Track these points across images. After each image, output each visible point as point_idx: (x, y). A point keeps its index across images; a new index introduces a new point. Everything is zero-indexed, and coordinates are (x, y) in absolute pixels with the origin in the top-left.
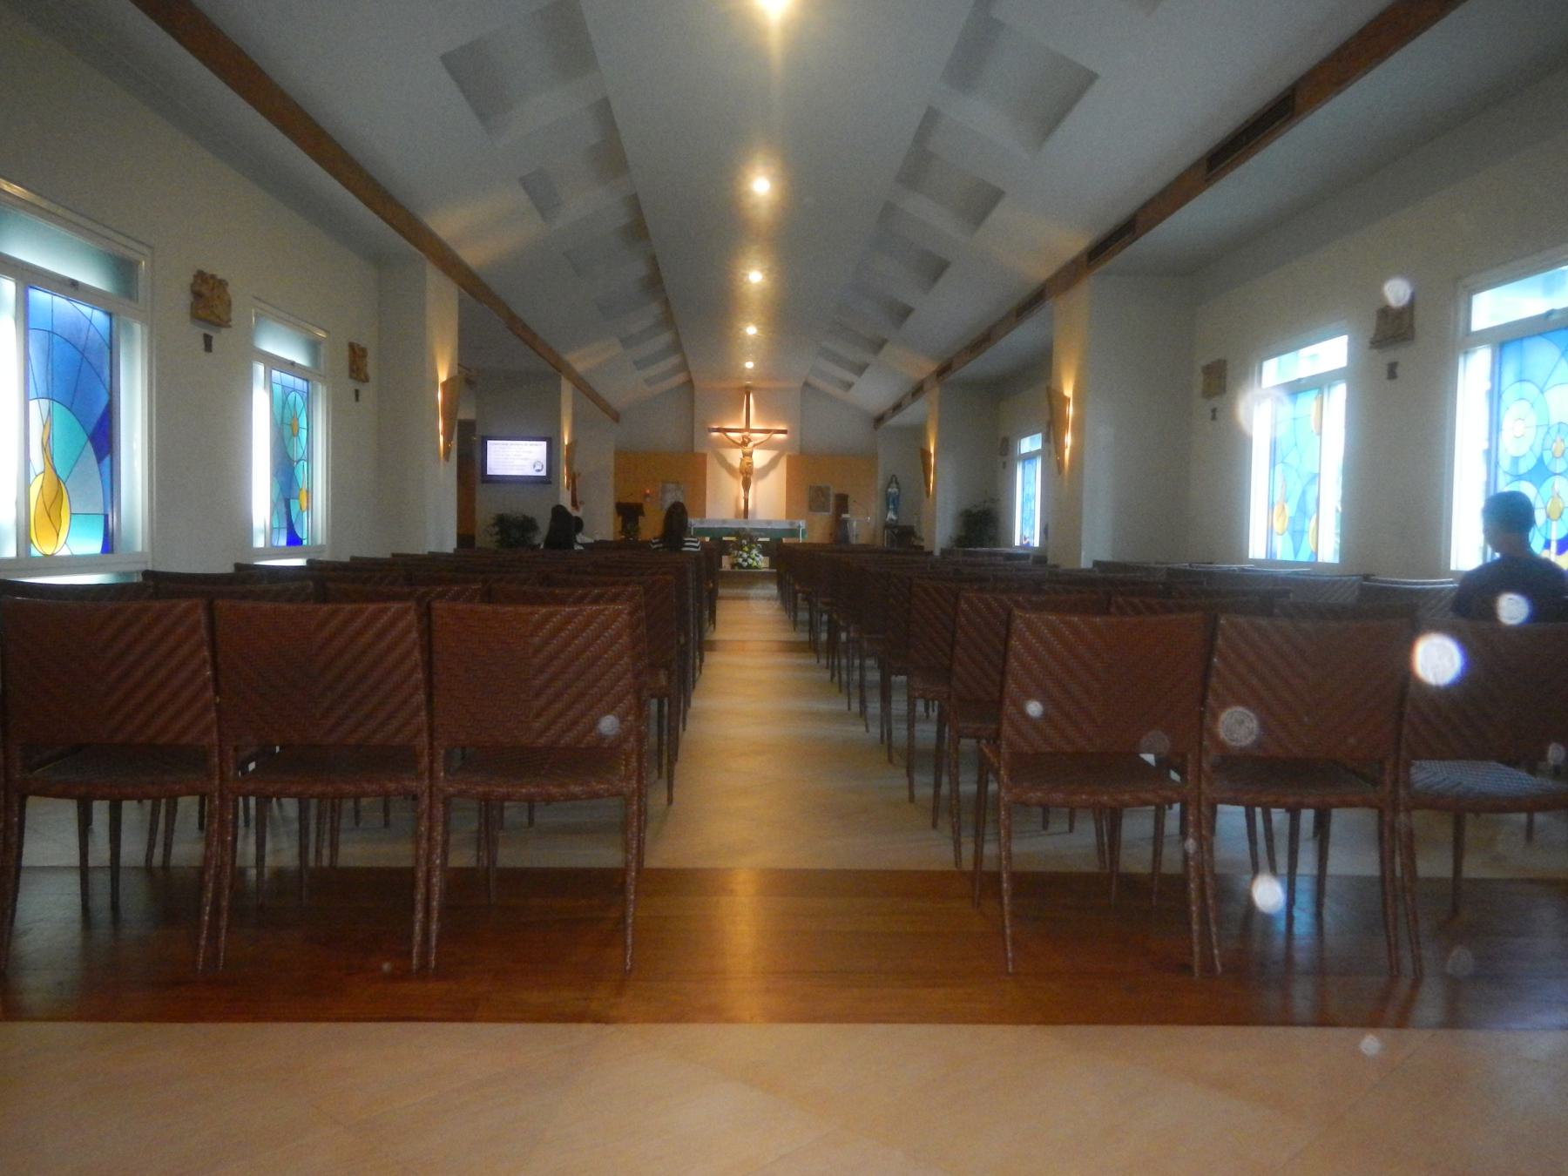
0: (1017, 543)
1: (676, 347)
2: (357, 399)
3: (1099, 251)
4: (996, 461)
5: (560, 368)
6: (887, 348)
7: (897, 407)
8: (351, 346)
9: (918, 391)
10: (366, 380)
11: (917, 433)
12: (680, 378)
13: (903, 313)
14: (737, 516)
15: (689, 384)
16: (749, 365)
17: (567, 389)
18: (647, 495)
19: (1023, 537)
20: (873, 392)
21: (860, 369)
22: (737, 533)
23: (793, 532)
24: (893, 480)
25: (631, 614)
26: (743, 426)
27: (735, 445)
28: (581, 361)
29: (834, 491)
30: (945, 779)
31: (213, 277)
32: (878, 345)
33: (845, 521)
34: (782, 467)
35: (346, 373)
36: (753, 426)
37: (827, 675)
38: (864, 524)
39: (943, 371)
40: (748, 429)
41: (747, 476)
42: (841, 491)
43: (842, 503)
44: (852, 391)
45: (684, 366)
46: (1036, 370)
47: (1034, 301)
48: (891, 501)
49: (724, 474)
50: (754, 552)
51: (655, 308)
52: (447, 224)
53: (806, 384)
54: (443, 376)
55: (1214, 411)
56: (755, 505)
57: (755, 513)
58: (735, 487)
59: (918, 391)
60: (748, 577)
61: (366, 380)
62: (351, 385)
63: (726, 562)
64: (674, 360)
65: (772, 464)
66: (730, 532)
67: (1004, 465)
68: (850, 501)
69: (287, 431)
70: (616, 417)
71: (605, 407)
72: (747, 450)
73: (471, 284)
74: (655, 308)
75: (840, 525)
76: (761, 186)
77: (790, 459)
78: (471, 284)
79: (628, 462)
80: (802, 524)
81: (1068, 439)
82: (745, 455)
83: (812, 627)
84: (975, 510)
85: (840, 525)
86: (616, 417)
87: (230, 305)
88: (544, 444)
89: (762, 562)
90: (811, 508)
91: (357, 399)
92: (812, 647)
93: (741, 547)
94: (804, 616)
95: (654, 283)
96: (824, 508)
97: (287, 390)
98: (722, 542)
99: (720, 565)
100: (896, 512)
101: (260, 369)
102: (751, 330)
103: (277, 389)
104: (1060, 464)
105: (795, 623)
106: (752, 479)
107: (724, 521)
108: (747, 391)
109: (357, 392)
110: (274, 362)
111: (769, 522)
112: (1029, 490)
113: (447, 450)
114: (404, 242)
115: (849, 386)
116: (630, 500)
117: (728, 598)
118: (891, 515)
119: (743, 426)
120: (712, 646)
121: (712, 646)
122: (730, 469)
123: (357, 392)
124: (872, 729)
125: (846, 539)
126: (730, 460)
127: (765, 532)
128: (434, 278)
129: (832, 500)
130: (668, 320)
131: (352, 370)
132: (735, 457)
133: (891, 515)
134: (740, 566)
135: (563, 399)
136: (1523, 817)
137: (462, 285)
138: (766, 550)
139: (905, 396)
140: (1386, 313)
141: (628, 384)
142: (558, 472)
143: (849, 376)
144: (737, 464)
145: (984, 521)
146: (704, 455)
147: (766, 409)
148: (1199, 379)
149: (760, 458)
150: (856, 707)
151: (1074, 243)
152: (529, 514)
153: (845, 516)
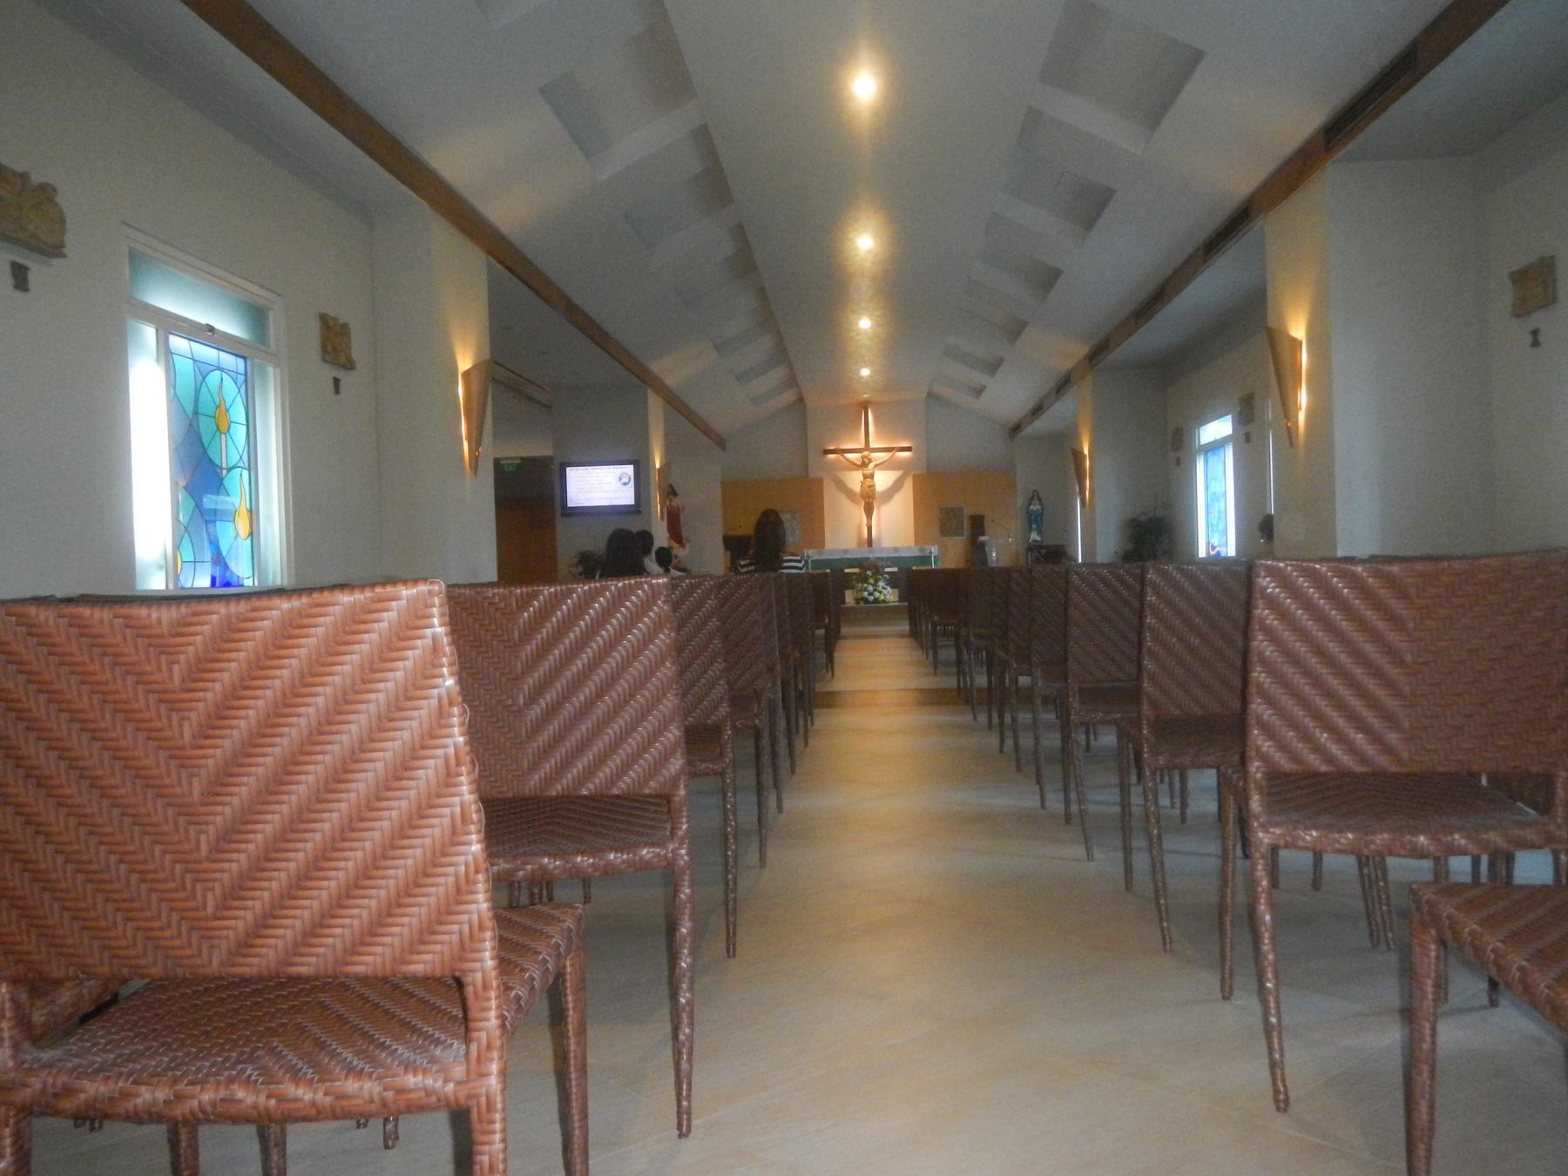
0: (1202, 553)
1: (781, 355)
2: (337, 391)
3: (1339, 129)
4: (1171, 453)
5: (644, 378)
6: (1028, 332)
7: (1038, 410)
8: (325, 320)
9: (1064, 384)
10: (349, 366)
11: (1063, 442)
12: (789, 396)
14: (860, 544)
17: (656, 408)
19: (1210, 546)
20: (1009, 394)
21: (993, 367)
22: (860, 563)
23: (925, 559)
24: (1035, 496)
26: (862, 445)
27: (855, 466)
28: (673, 369)
29: (968, 511)
30: (1139, 842)
31: (24, 176)
32: (1015, 330)
33: (983, 545)
34: (908, 486)
35: (318, 357)
37: (994, 741)
39: (1095, 356)
40: (867, 447)
41: (869, 501)
43: (978, 525)
44: (985, 396)
45: (792, 381)
46: (1249, 318)
47: (1240, 220)
48: (1034, 520)
49: (844, 500)
50: (881, 584)
51: (767, 343)
52: (455, 159)
53: (930, 395)
54: (464, 363)
55: (1535, 333)
57: (879, 539)
59: (1064, 384)
60: (875, 613)
61: (349, 366)
62: (329, 372)
63: (850, 598)
64: (778, 373)
65: (897, 486)
67: (1178, 462)
68: (987, 524)
69: (206, 426)
70: (721, 443)
71: (708, 432)
72: (868, 472)
73: (503, 254)
74: (767, 343)
75: (976, 549)
76: (865, 243)
77: (916, 479)
78: (503, 254)
80: (934, 550)
81: (1303, 397)
82: (865, 477)
83: (959, 666)
86: (721, 443)
87: (63, 221)
89: (889, 595)
91: (337, 391)
92: (962, 697)
93: (865, 580)
94: (948, 654)
95: (744, 264)
96: (957, 532)
97: (203, 370)
100: (1040, 532)
101: (149, 333)
103: (185, 367)
105: (936, 663)
106: (875, 505)
107: (846, 551)
108: (865, 405)
109: (336, 381)
110: (168, 324)
111: (896, 550)
112: (1216, 487)
113: (475, 460)
114: (388, 176)
115: (979, 391)
117: (855, 637)
118: (1034, 536)
119: (862, 445)
120: (830, 701)
121: (830, 701)
123: (336, 381)
124: (1049, 796)
127: (893, 561)
128: (442, 237)
129: (966, 525)
130: (767, 318)
131: (324, 351)
132: (855, 480)
133: (1034, 536)
134: (866, 601)
135: (651, 418)
137: (489, 252)
138: (893, 581)
141: (728, 406)
142: (648, 503)
143: (980, 378)
144: (857, 489)
145: (1156, 532)
146: (820, 481)
147: (884, 426)
148: (1505, 296)
149: (883, 480)
150: (1055, 802)
151: (1299, 121)
153: (982, 538)
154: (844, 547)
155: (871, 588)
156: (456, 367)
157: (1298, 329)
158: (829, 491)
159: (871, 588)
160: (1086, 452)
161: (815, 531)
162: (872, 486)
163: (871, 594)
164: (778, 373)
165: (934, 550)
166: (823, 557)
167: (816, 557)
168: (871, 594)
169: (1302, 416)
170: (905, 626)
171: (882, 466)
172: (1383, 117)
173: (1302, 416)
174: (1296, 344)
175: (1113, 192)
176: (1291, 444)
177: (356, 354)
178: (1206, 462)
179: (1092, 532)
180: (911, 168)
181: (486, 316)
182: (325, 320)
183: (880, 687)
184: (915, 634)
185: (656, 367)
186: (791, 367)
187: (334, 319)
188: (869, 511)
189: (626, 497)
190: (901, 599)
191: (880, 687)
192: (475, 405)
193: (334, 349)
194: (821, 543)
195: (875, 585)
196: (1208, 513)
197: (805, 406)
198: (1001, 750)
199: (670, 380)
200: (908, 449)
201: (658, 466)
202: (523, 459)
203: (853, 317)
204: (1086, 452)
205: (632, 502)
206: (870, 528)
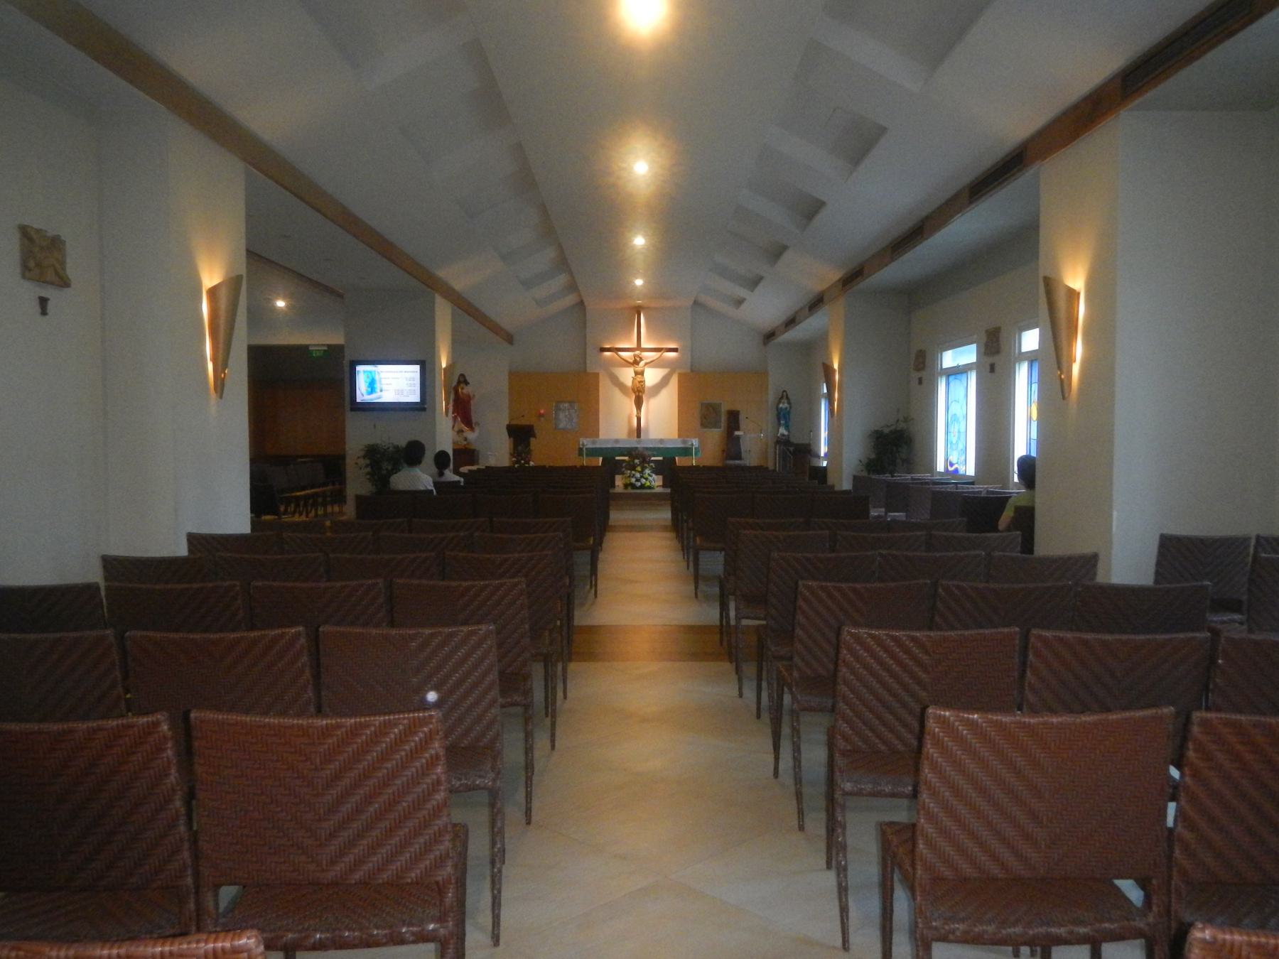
0: (940, 467)
4: (920, 372)
5: (432, 284)
6: (788, 256)
7: (791, 322)
8: (26, 233)
9: (817, 303)
11: (812, 350)
12: (570, 300)
13: (810, 209)
16: (639, 282)
17: (443, 314)
18: (541, 415)
19: (948, 463)
20: (766, 307)
21: (754, 283)
22: (631, 452)
23: (686, 451)
24: (784, 396)
26: (634, 345)
28: (460, 276)
29: (725, 408)
32: (776, 253)
33: (738, 437)
34: (674, 382)
36: (644, 345)
38: (756, 443)
39: (852, 278)
40: (639, 347)
44: (744, 306)
45: (573, 287)
47: (1012, 164)
48: (782, 416)
49: (617, 393)
50: (647, 471)
51: (550, 253)
53: (696, 303)
54: (211, 277)
56: (647, 422)
58: (628, 404)
59: (817, 303)
60: (642, 498)
61: (63, 283)
63: (619, 481)
64: (561, 280)
65: (664, 382)
66: (622, 451)
68: (742, 417)
70: (509, 339)
71: (496, 329)
72: (639, 368)
75: (732, 445)
77: (680, 375)
78: (261, 160)
79: (523, 383)
80: (695, 442)
81: (1079, 349)
82: (636, 373)
84: (886, 431)
85: (732, 445)
86: (509, 339)
89: (656, 481)
90: (703, 425)
93: (633, 468)
96: (716, 425)
98: (616, 461)
99: (613, 485)
100: (787, 428)
102: (639, 241)
104: (1064, 385)
107: (617, 441)
108: (638, 310)
109: (43, 302)
111: (661, 441)
113: (220, 385)
115: (740, 302)
116: (524, 422)
118: (782, 431)
119: (634, 345)
122: (622, 387)
123: (43, 302)
126: (622, 379)
127: (658, 451)
129: (724, 418)
132: (627, 375)
133: (782, 431)
134: (633, 486)
137: (245, 160)
139: (801, 309)
141: (513, 308)
143: (742, 292)
144: (629, 383)
145: (899, 443)
146: (597, 375)
149: (652, 376)
151: (1091, 63)
152: (413, 438)
153: (737, 433)
155: (638, 475)
157: (1076, 279)
158: (604, 384)
159: (638, 475)
160: (836, 366)
162: (642, 382)
163: (638, 480)
164: (561, 280)
165: (695, 442)
166: (598, 446)
167: (590, 446)
168: (638, 480)
169: (1076, 369)
170: (665, 515)
171: (650, 364)
172: (1196, 64)
173: (1076, 369)
174: (1073, 294)
175: (883, 130)
176: (1064, 398)
177: (71, 271)
178: (948, 384)
179: (833, 438)
180: (685, 89)
181: (243, 230)
182: (26, 233)
183: (642, 584)
184: (677, 526)
185: (442, 274)
186: (571, 274)
187: (38, 231)
188: (639, 403)
189: (412, 395)
190: (664, 486)
191: (642, 584)
192: (222, 321)
193: (38, 265)
194: (596, 433)
195: (641, 472)
196: (947, 432)
197: (584, 309)
198: (776, 773)
199: (458, 285)
201: (444, 365)
202: (329, 346)
204: (836, 366)
205: (415, 397)
206: (639, 419)
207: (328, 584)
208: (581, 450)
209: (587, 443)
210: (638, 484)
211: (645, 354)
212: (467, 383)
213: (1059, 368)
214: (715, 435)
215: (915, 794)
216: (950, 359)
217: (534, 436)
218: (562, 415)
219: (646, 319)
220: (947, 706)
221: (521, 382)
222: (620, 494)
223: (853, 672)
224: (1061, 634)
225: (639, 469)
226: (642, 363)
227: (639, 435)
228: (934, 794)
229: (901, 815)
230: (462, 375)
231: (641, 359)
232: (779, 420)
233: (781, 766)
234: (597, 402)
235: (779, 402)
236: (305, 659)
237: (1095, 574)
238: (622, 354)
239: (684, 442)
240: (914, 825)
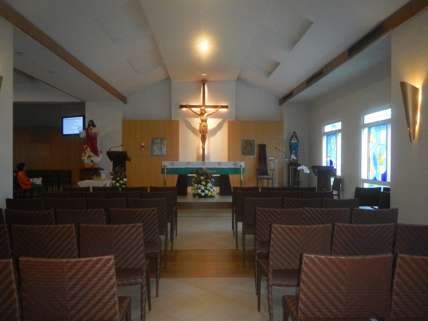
14: (198, 158)
15: (168, 79)
18: (142, 147)
22: (199, 172)
23: (237, 171)
24: (294, 135)
25: (115, 259)
26: (201, 103)
29: (258, 142)
34: (225, 127)
41: (204, 134)
42: (261, 143)
48: (293, 148)
49: (190, 133)
50: (209, 185)
58: (197, 140)
65: (219, 127)
66: (192, 171)
70: (124, 99)
77: (229, 123)
80: (243, 164)
82: (202, 121)
86: (124, 99)
88: (82, 118)
90: (243, 153)
93: (199, 182)
96: (251, 153)
100: (296, 156)
104: (411, 136)
106: (207, 138)
107: (188, 163)
108: (204, 82)
111: (219, 163)
118: (293, 157)
119: (201, 103)
122: (193, 130)
125: (298, 183)
127: (217, 170)
132: (196, 123)
133: (293, 157)
134: (200, 196)
136: (348, 209)
140: (161, 140)
144: (197, 127)
146: (178, 121)
147: (216, 93)
149: (212, 123)
154: (187, 160)
155: (203, 188)
156: (230, 186)
158: (183, 129)
159: (203, 188)
161: (173, 153)
162: (206, 126)
163: (203, 191)
167: (169, 167)
168: (203, 191)
169: (417, 127)
173: (417, 127)
174: (415, 90)
188: (203, 139)
195: (205, 186)
200: (226, 107)
203: (198, 46)
206: (204, 149)
207: (56, 226)
208: (163, 170)
209: (168, 164)
210: (203, 194)
211: (207, 110)
212: (94, 126)
213: (409, 126)
214: (252, 159)
215: (298, 285)
216: (328, 128)
217: (129, 160)
218: (155, 147)
219: (207, 86)
220: (310, 253)
221: (130, 126)
222: (191, 203)
223: (308, 277)
224: (344, 225)
225: (204, 183)
226: (206, 115)
227: (203, 160)
228: (305, 284)
229: (292, 291)
230: (91, 121)
231: (205, 112)
232: (291, 150)
233: (238, 244)
234: (178, 141)
235: (291, 139)
236: (75, 240)
237: (397, 218)
238: (195, 109)
239: (235, 164)
240: (298, 297)
